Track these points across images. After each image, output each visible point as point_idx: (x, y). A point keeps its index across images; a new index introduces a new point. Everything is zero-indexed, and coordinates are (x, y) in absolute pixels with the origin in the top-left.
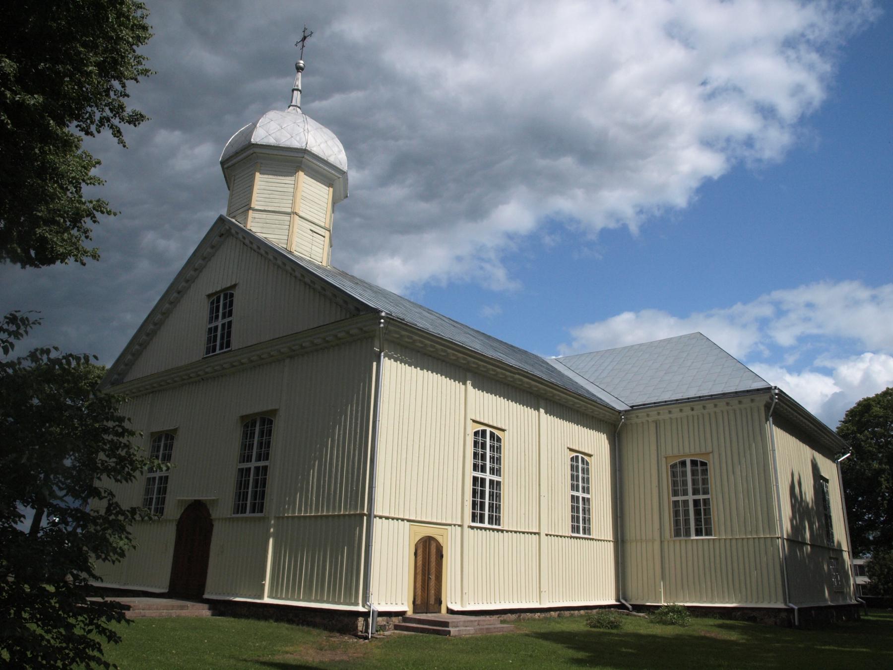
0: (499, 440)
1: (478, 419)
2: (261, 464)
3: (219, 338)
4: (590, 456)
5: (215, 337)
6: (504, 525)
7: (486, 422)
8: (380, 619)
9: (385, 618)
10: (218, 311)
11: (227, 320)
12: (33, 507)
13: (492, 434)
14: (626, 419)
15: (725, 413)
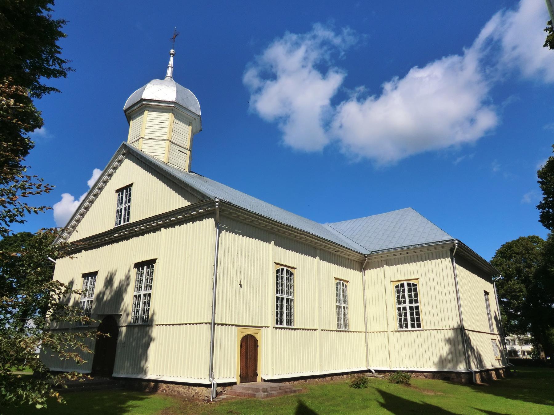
0: (292, 274)
1: (280, 262)
2: (147, 292)
3: (123, 212)
4: (348, 282)
5: (121, 215)
6: (296, 325)
7: (284, 264)
8: (218, 388)
9: (222, 387)
10: (122, 199)
11: (128, 205)
12: (491, 261)
13: (288, 271)
14: (369, 259)
15: (427, 255)
